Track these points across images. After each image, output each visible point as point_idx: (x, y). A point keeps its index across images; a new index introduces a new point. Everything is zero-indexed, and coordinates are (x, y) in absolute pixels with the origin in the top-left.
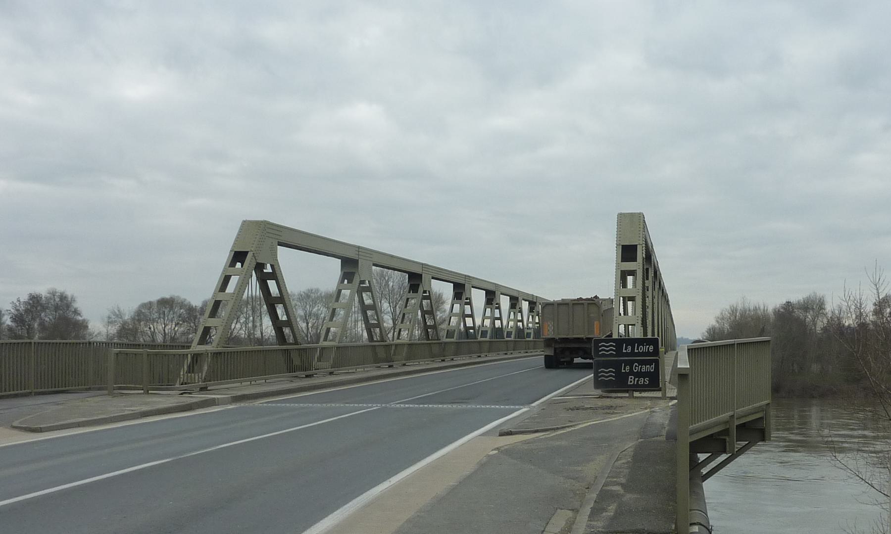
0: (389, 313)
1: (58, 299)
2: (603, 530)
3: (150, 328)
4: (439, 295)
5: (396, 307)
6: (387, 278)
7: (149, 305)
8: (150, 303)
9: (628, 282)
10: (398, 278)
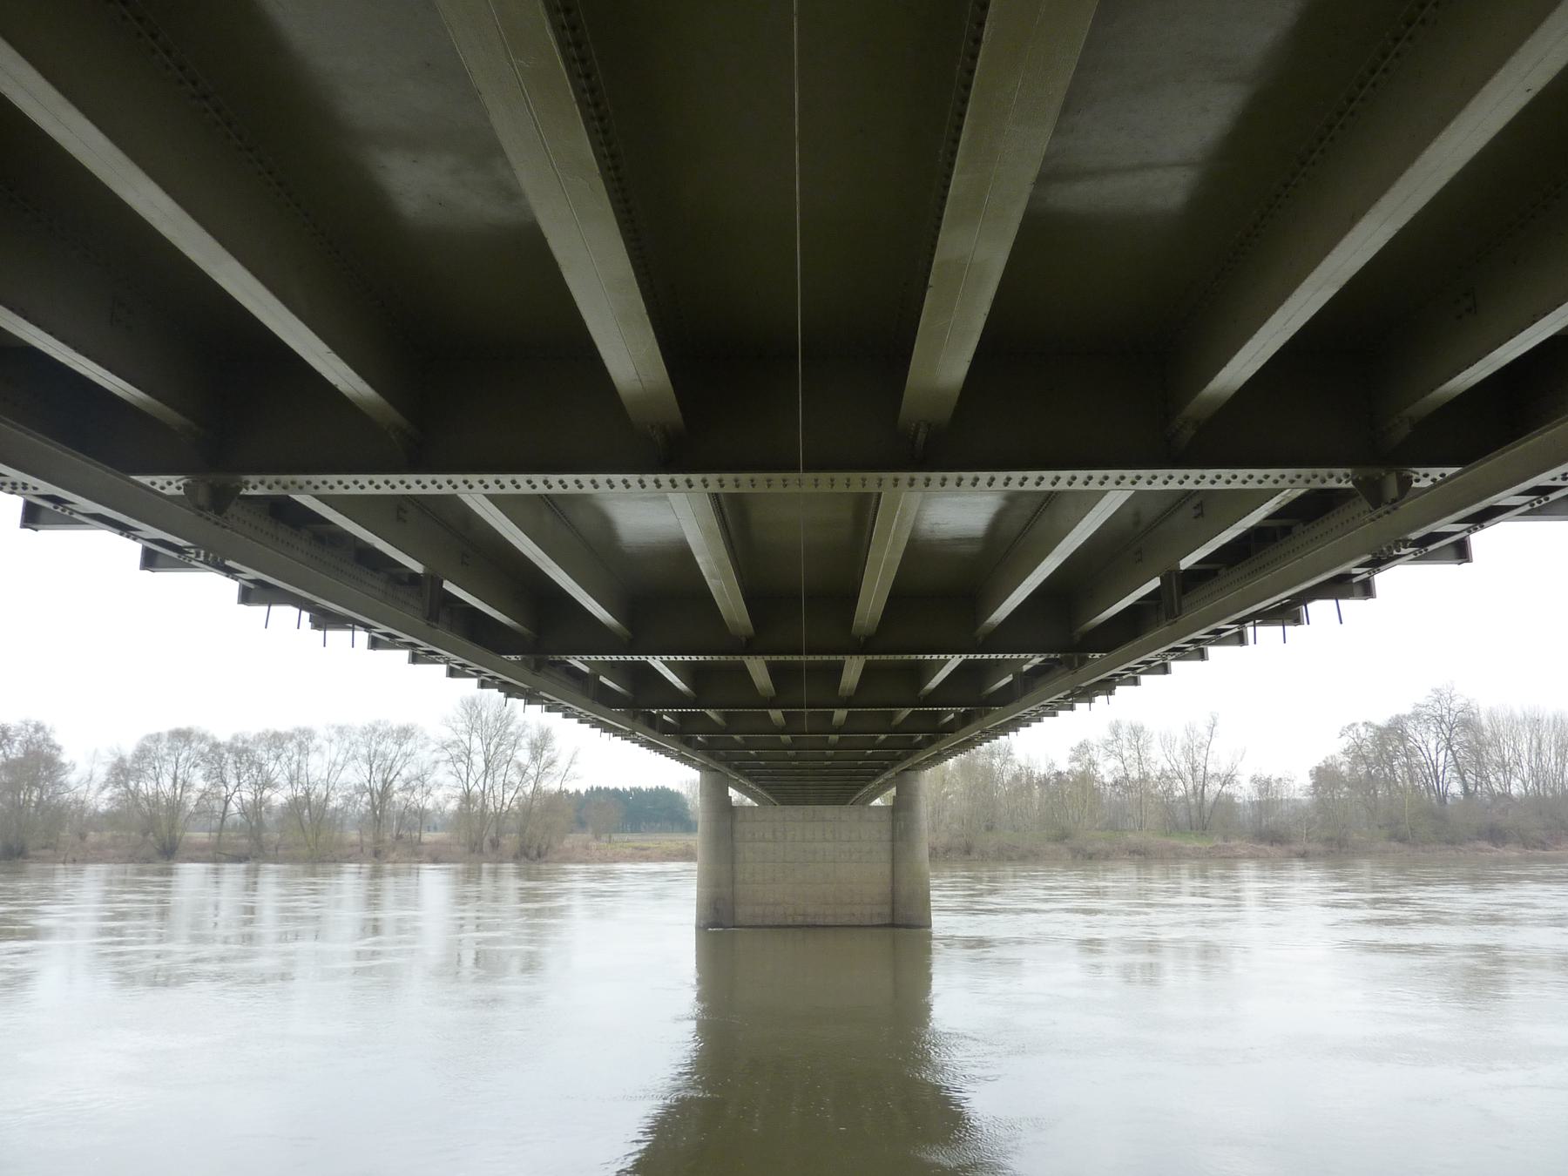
0: (480, 752)
1: (33, 730)
2: (570, 867)
3: (155, 768)
4: (547, 730)
5: (489, 744)
6: (479, 708)
7: (157, 738)
8: (159, 734)
9: (1032, 590)
10: (495, 707)
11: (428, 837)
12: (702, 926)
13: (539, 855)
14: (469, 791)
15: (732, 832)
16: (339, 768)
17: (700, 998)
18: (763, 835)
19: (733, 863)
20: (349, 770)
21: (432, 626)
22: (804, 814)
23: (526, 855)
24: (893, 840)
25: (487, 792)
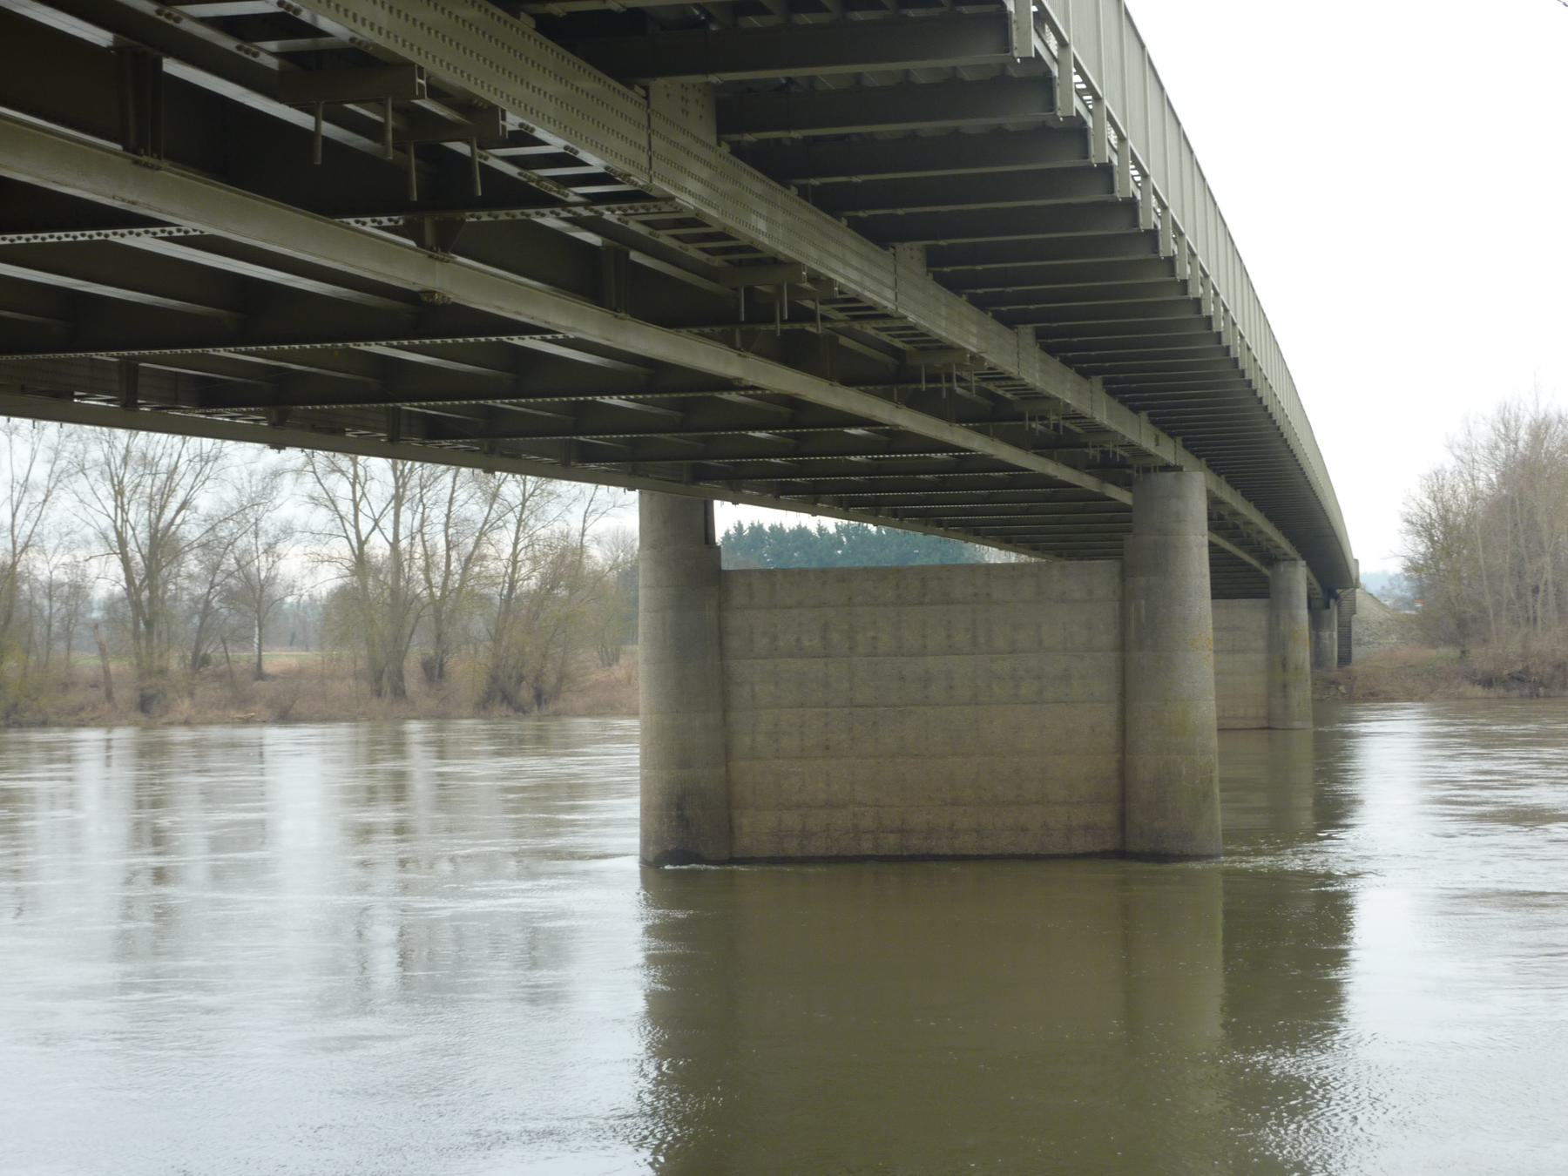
11: (279, 659)
12: (651, 859)
13: (539, 697)
14: (361, 543)
15: (721, 634)
16: (40, 497)
17: (660, 1050)
18: (798, 640)
19: (726, 710)
20: (64, 502)
21: (146, 165)
22: (898, 586)
23: (507, 699)
24: (1123, 647)
25: (404, 544)
